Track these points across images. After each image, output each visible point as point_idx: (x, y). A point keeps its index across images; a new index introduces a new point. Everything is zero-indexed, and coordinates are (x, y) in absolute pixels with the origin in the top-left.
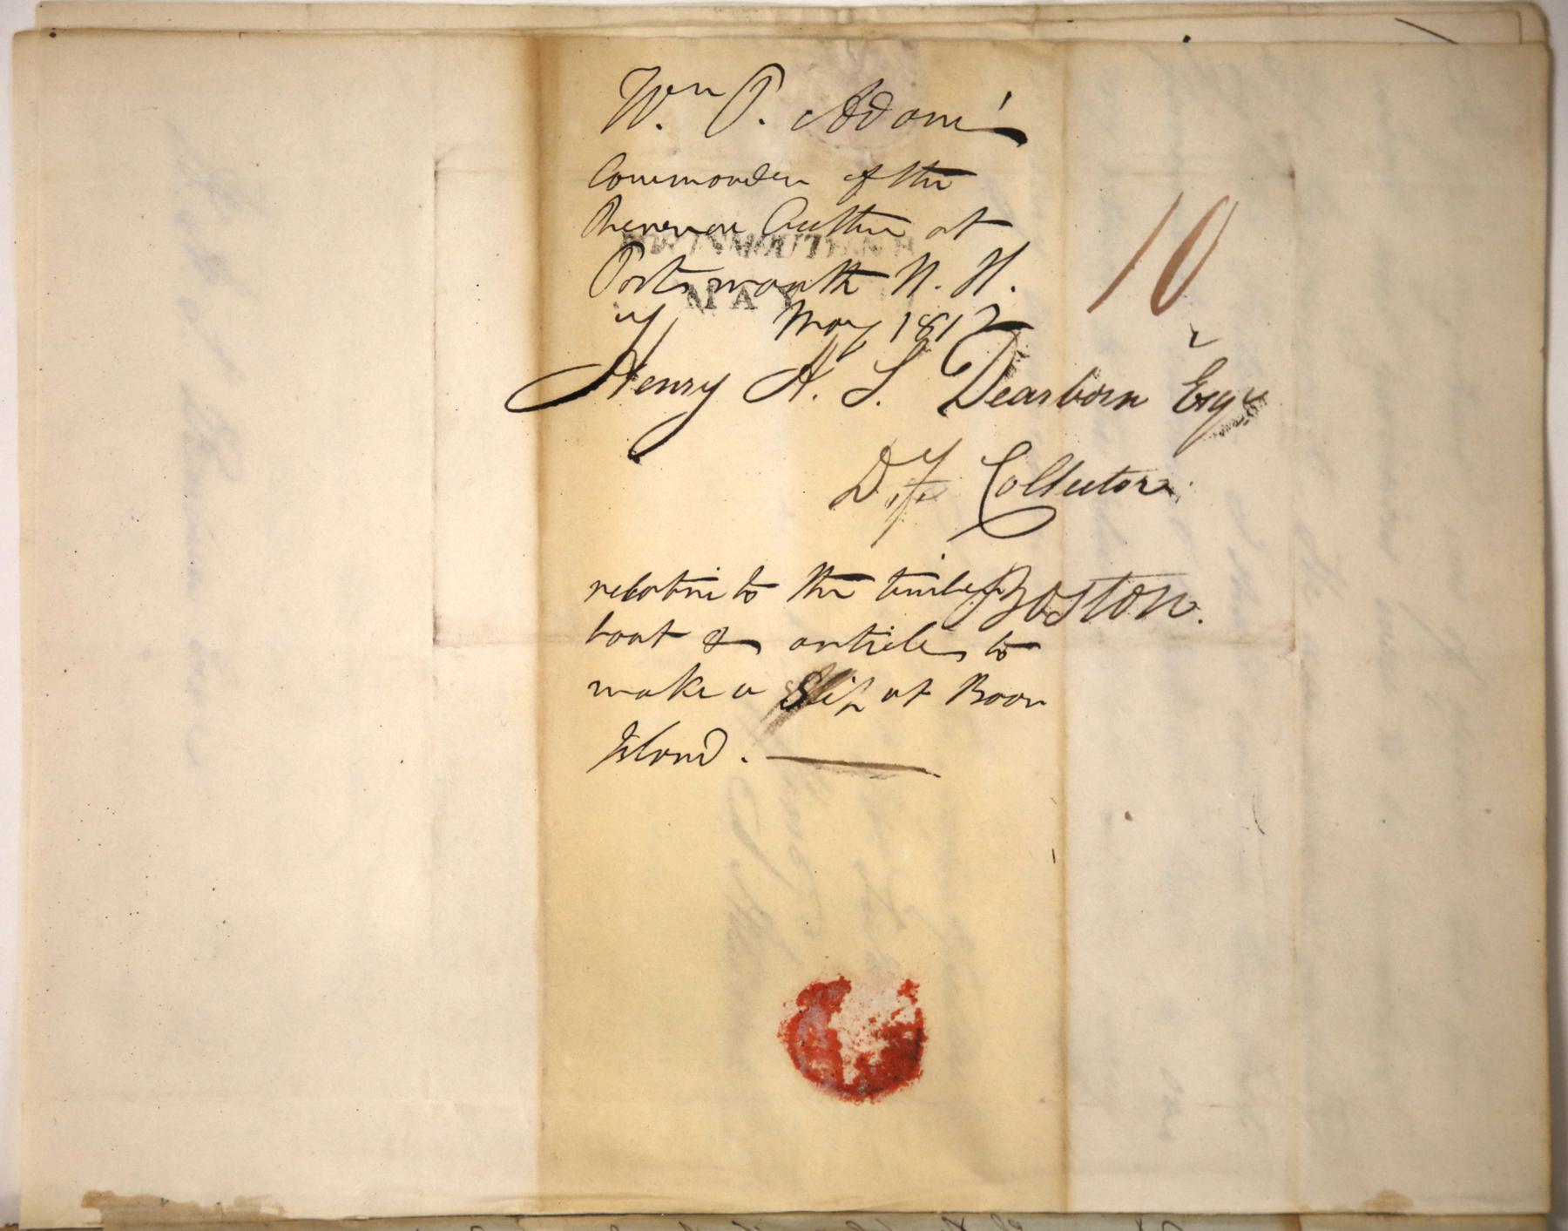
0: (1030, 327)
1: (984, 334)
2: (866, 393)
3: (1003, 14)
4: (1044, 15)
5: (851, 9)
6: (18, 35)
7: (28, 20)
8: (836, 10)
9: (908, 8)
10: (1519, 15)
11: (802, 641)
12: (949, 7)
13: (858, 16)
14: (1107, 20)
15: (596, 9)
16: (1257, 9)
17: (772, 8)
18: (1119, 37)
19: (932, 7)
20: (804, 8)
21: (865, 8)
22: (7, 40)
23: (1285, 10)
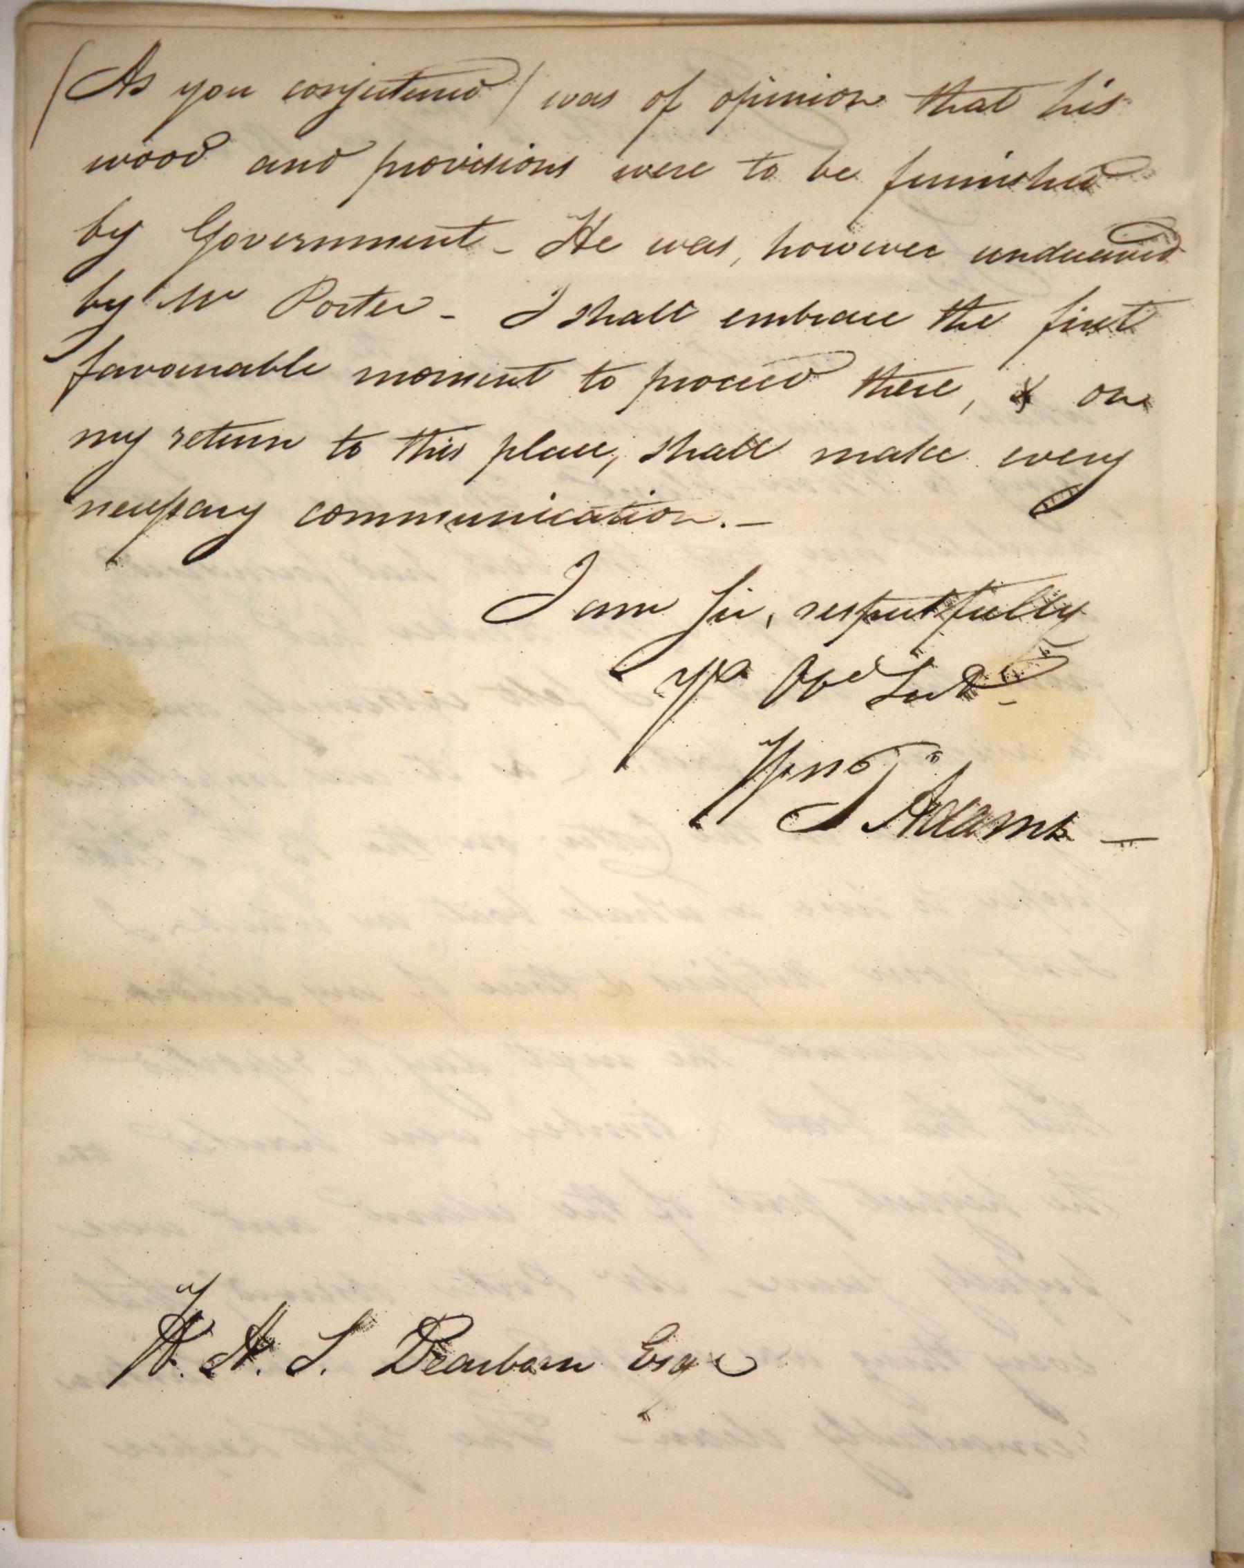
0: (883, 656)
1: (686, 628)
2: (550, 599)
3: (20, 548)
4: (21, 508)
5: (14, 701)
6: (20, 1532)
7: (10, 1526)
8: (15, 716)
9: (13, 644)
10: (30, 25)
11: (1047, 328)
12: (13, 602)
13: (20, 695)
14: (27, 435)
15: (10, 956)
16: (20, 294)
17: (11, 780)
18: (413, 1363)
19: (13, 619)
20: (12, 747)
21: (13, 687)
22: (21, 1543)
23: (21, 266)
